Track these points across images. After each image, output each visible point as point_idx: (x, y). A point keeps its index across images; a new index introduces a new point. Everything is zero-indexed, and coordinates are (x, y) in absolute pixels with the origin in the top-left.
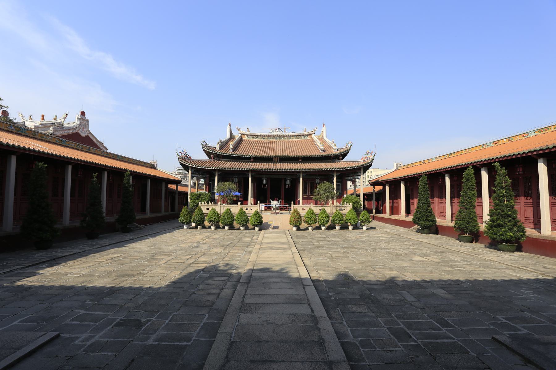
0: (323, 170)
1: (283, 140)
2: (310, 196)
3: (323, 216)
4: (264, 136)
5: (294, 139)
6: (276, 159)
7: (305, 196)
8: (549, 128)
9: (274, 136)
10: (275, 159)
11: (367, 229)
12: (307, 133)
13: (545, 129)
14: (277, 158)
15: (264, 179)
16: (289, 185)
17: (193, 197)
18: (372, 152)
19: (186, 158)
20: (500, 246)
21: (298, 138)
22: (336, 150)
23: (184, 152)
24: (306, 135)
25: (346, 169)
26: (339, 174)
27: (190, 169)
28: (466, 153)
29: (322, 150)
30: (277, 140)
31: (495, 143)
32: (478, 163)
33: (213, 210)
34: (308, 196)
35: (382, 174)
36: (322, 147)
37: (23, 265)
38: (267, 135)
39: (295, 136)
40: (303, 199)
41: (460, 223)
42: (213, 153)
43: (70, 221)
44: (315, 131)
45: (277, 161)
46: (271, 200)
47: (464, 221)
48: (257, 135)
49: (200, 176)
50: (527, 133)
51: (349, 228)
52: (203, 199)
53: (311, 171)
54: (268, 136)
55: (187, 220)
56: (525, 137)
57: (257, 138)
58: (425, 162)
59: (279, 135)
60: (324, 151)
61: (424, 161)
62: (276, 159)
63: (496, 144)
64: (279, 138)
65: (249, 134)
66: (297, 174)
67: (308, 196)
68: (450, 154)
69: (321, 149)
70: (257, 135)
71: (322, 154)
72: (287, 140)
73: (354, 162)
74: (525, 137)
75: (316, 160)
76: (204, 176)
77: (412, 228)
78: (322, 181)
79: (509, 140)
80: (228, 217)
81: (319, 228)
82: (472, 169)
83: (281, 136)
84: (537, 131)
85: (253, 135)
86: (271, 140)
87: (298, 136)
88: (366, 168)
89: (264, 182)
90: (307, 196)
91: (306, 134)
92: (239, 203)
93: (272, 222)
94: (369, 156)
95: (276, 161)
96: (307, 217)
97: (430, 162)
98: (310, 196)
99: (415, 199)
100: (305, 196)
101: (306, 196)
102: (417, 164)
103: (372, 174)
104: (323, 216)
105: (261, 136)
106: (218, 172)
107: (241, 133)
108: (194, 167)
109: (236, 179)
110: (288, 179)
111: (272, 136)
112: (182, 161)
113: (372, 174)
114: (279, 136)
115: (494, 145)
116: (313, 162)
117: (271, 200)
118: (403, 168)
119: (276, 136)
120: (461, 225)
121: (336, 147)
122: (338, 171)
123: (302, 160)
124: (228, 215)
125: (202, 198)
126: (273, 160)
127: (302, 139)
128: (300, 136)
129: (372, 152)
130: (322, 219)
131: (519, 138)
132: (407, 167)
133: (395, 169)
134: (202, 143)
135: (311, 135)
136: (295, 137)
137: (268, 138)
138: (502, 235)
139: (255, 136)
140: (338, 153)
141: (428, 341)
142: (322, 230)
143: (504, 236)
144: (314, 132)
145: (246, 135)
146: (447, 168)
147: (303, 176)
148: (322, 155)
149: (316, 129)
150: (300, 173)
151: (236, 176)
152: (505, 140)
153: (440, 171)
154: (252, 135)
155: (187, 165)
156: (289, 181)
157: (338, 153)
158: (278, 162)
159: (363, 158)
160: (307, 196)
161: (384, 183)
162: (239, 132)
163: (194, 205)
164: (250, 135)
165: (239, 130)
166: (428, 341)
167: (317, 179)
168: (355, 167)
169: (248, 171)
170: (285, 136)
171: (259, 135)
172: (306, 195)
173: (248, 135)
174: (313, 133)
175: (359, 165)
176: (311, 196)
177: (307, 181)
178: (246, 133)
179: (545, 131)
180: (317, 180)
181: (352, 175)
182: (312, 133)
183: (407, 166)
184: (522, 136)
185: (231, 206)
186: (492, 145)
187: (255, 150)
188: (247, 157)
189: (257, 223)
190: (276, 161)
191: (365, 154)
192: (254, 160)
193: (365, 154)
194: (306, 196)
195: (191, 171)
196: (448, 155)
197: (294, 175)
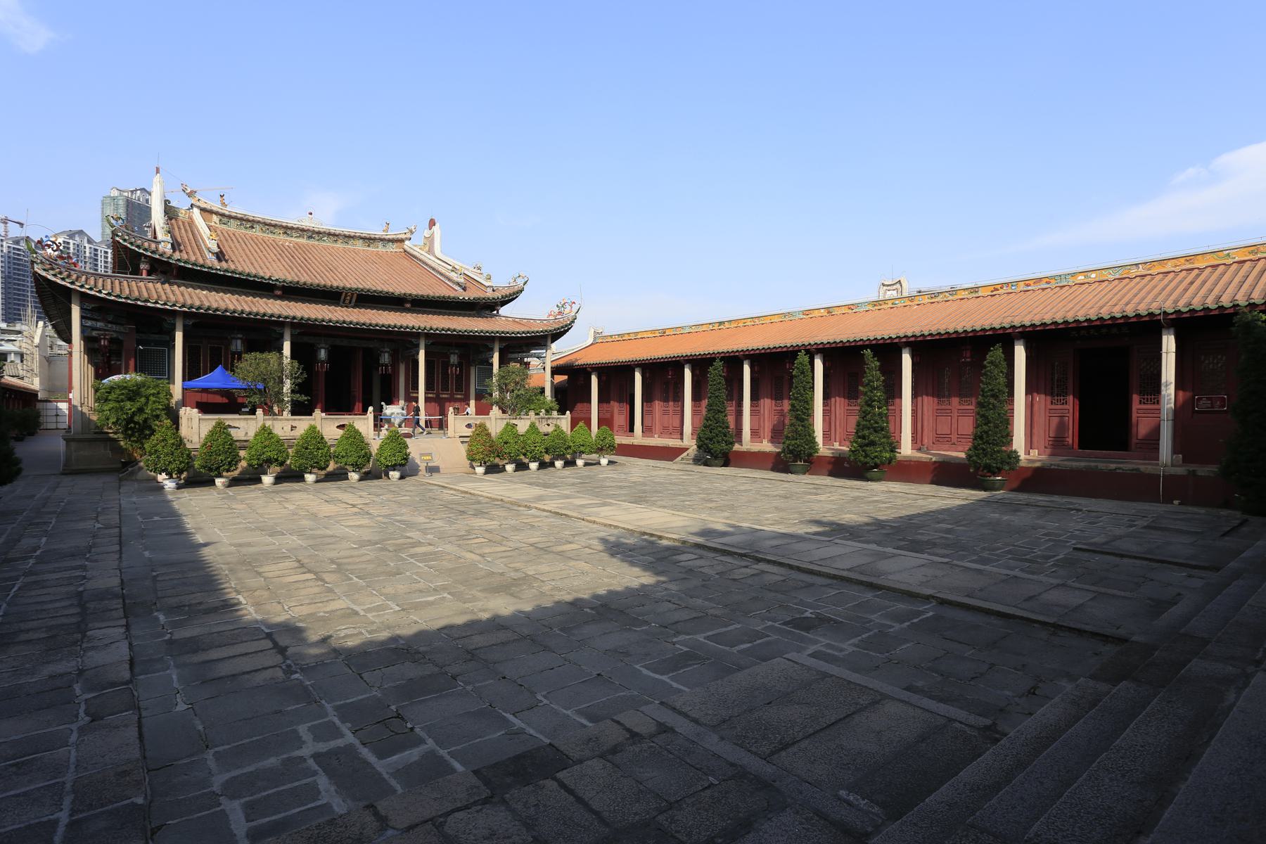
0: (477, 334)
1: (327, 243)
2: (441, 396)
3: (537, 440)
4: (275, 226)
5: (359, 245)
6: (348, 298)
7: (430, 395)
8: (886, 302)
9: (303, 230)
10: (346, 296)
11: (586, 464)
12: (391, 234)
13: (880, 302)
14: (353, 294)
15: (324, 348)
16: (386, 366)
17: (109, 393)
18: (574, 303)
19: (60, 262)
20: (869, 475)
21: (369, 246)
22: (489, 290)
23: (54, 242)
24: (389, 240)
25: (524, 335)
26: (504, 344)
27: (75, 299)
28: (753, 323)
29: (460, 286)
30: (311, 242)
31: (806, 312)
32: (815, 347)
33: (265, 432)
34: (452, 395)
35: (568, 351)
36: (461, 278)
37: (756, 572)
38: (284, 224)
39: (362, 238)
40: (426, 402)
41: (795, 443)
42: (146, 256)
43: (381, 478)
44: (412, 232)
45: (350, 303)
46: (383, 403)
47: (803, 439)
48: (253, 221)
49: (110, 326)
50: (857, 305)
51: (530, 467)
52: (152, 398)
53: (449, 334)
54: (287, 228)
55: (181, 462)
56: (854, 311)
57: (253, 227)
58: (665, 333)
59: (316, 230)
60: (464, 289)
61: (664, 331)
62: (348, 298)
63: (807, 315)
64: (317, 238)
65: (227, 213)
66: (413, 340)
67: (452, 395)
68: (721, 323)
69: (458, 284)
70: (251, 218)
71: (462, 295)
72: (339, 245)
73: (532, 321)
74: (854, 311)
75: (242, 288)
76: (122, 329)
77: (679, 458)
78: (252, 347)
79: (829, 312)
80: (318, 449)
81: (340, 475)
82: (805, 355)
83: (325, 232)
84: (869, 303)
85: (241, 219)
86: (293, 239)
87: (370, 239)
88: (557, 335)
89: (323, 354)
90: (463, 397)
91: (388, 237)
92: (259, 412)
93: (430, 458)
94: (567, 310)
95: (347, 302)
96: (506, 443)
97: (678, 333)
98: (441, 396)
99: (657, 402)
100: (430, 395)
101: (446, 396)
102: (645, 336)
103: (560, 350)
104: (537, 440)
105: (265, 224)
106: (426, 339)
107: (198, 204)
108: (102, 296)
109: (239, 342)
110: (386, 352)
111: (298, 228)
112: (52, 272)
113: (560, 350)
114: (319, 233)
115: (804, 316)
116: (310, 300)
117: (383, 403)
118: (610, 339)
119: (308, 230)
120: (798, 446)
121: (497, 280)
122: (502, 339)
123: (412, 306)
124: (319, 443)
125: (148, 399)
126: (339, 299)
127: (380, 248)
128: (374, 239)
129: (574, 303)
130: (535, 447)
131: (844, 310)
132: (620, 339)
133: (590, 341)
134: (113, 221)
135: (402, 241)
136: (361, 241)
137: (285, 233)
138: (876, 457)
139: (248, 220)
140: (498, 298)
141: (8, 763)
142: (555, 467)
143: (878, 459)
144: (408, 236)
145: (217, 213)
146: (753, 350)
147: (292, 336)
148: (464, 298)
149: (413, 228)
150: (494, 342)
151: (240, 336)
152: (822, 311)
153: (737, 354)
154: (235, 218)
155: (63, 283)
156: (386, 355)
157: (498, 298)
158: (352, 304)
159: (553, 313)
160: (434, 396)
161: (588, 369)
162: (193, 202)
163: (118, 419)
164: (230, 217)
165: (191, 194)
166: (8, 763)
167: (454, 353)
168: (542, 331)
169: (282, 324)
170: (334, 235)
171: (259, 222)
172: (433, 393)
173: (223, 215)
174: (406, 239)
175: (550, 328)
176: (444, 396)
177: (435, 359)
178: (215, 209)
179: (881, 305)
180: (452, 356)
181: (525, 349)
182: (403, 236)
183: (622, 338)
184: (849, 308)
185: (295, 420)
186: (802, 316)
187: (313, 265)
188: (268, 283)
189: (402, 460)
190: (347, 302)
191: (557, 306)
192: (283, 293)
193: (557, 306)
194: (446, 396)
195: (82, 309)
196: (718, 324)
197: (403, 342)
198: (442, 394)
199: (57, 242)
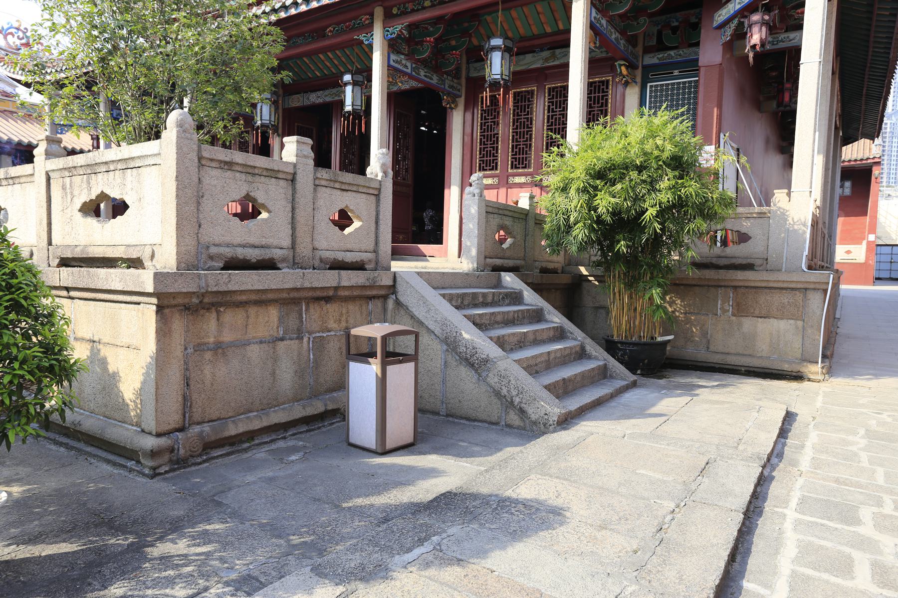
23: (18, 29)
198: (514, 175)
199: (22, 28)
